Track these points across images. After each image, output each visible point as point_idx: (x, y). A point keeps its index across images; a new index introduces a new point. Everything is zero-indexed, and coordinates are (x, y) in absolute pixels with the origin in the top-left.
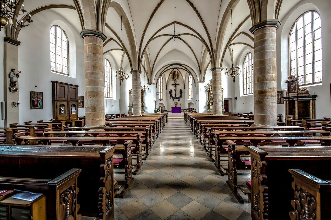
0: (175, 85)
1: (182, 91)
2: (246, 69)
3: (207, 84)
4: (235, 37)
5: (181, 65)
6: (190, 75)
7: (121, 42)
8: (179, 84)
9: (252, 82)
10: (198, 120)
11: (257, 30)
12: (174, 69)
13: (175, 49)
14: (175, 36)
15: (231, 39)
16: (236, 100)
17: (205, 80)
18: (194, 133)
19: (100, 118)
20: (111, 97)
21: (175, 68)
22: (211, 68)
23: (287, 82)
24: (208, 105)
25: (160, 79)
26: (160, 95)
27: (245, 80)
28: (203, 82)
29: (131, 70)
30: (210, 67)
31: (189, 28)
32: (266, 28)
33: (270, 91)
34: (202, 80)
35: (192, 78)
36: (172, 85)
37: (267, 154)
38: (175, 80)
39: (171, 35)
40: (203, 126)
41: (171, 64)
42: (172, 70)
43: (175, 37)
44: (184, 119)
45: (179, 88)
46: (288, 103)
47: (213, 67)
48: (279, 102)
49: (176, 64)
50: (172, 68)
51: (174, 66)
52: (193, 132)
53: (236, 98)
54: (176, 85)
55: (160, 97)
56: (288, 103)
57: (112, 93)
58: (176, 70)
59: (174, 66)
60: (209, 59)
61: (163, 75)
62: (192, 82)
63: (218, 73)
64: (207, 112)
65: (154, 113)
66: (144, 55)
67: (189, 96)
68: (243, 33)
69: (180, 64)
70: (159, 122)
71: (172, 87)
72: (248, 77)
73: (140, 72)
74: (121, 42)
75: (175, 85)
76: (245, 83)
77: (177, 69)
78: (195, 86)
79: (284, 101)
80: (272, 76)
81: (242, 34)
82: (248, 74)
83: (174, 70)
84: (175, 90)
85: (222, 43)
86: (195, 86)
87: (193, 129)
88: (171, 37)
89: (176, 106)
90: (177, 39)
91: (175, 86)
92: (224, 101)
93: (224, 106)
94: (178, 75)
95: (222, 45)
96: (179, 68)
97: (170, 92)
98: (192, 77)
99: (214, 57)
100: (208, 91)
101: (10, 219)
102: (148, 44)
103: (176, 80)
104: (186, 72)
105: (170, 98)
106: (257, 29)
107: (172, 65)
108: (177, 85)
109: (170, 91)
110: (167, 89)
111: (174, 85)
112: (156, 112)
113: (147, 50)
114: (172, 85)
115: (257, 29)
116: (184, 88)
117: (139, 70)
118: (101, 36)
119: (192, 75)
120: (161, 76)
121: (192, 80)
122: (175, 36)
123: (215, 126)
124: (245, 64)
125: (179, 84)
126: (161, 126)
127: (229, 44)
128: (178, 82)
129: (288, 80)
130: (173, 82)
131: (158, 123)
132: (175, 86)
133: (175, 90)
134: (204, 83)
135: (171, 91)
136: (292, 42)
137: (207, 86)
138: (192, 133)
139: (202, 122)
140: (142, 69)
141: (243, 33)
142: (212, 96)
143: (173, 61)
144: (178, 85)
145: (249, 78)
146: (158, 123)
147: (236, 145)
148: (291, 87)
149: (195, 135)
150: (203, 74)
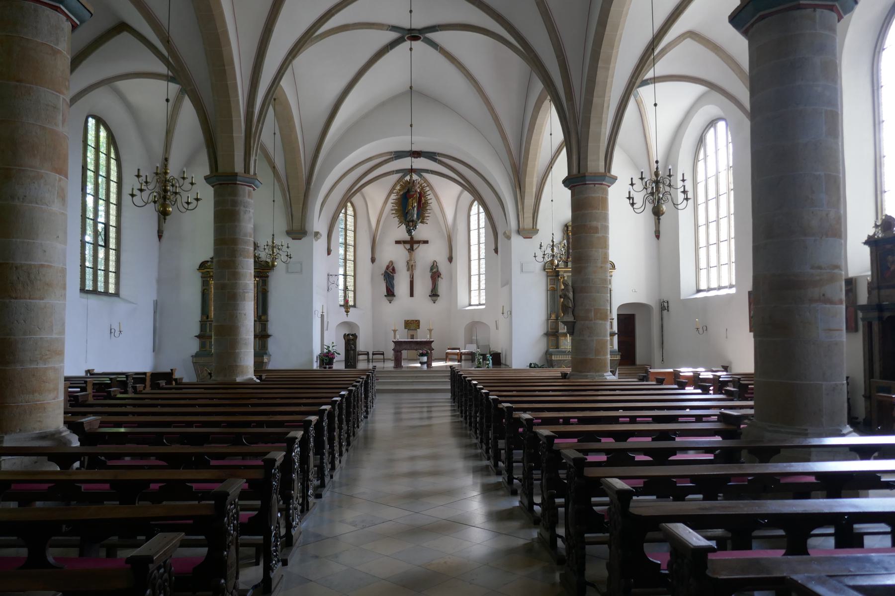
0: (411, 244)
1: (439, 270)
2: (704, 183)
3: (546, 242)
4: (664, 51)
5: (435, 160)
6: (476, 203)
7: (167, 41)
8: (426, 242)
9: (728, 240)
10: (500, 399)
11: (763, 18)
12: (404, 176)
13: (411, 88)
14: (414, 35)
15: (648, 56)
16: (665, 312)
17: (538, 227)
18: (496, 465)
19: (36, 394)
20: (112, 290)
21: (412, 171)
22: (565, 174)
23: (871, 242)
24: (552, 334)
25: (346, 213)
26: (341, 286)
27: (702, 231)
28: (528, 232)
29: (208, 172)
30: (561, 169)
31: (447, 167)
32: (797, 13)
33: (818, 278)
34: (527, 223)
35: (483, 216)
36: (397, 242)
37: (460, 372)
38: (409, 222)
39: (394, 28)
40: (484, 395)
41: (396, 152)
42: (397, 176)
43: (415, 38)
44: (449, 395)
45: (427, 255)
46: (876, 328)
47: (575, 171)
48: (852, 327)
49: (416, 154)
50: (398, 172)
51: (405, 163)
52: (466, 423)
53: (666, 304)
54: (415, 246)
55: (341, 293)
56: (876, 328)
57: (83, 267)
58: (415, 177)
59: (405, 163)
60: (559, 135)
61: (357, 199)
62: (483, 231)
63: (593, 195)
64: (529, 367)
65: (316, 366)
66: (271, 108)
67: (470, 291)
68: (692, 35)
69: (431, 156)
70: (337, 413)
71: (394, 253)
72: (712, 217)
73: (252, 182)
74: (167, 41)
75: (411, 244)
76: (702, 242)
77: (421, 176)
78: (496, 251)
79: (860, 324)
80: (827, 215)
81: (688, 41)
82: (712, 204)
83: (408, 178)
84: (411, 267)
85: (610, 72)
86: (496, 251)
87: (466, 413)
88: (393, 35)
89: (412, 337)
90: (418, 45)
91: (408, 246)
92: (618, 315)
93: (616, 336)
94: (423, 201)
95: (609, 80)
96: (427, 171)
97: (386, 272)
98: (481, 210)
99: (579, 128)
100: (552, 272)
101: (153, 523)
102: (291, 61)
103: (413, 221)
104: (459, 188)
105: (385, 298)
106: (762, 13)
107: (399, 155)
108: (419, 242)
109: (388, 267)
110: (373, 260)
111: (405, 242)
112: (176, 380)
113: (285, 83)
114: (397, 242)
115: (762, 13)
116: (450, 259)
117: (249, 172)
118: (253, 184)
119: (483, 203)
120: (349, 204)
121: (482, 224)
122: (414, 35)
123: (567, 421)
124: (701, 165)
125: (426, 242)
126: (348, 424)
127: (636, 80)
128: (422, 231)
129: (875, 234)
130: (401, 232)
131: (337, 408)
132: (411, 250)
133: (411, 267)
134: (537, 239)
135: (394, 269)
136: (714, 177)
137: (549, 251)
138: (458, 413)
139: (514, 406)
140: (258, 167)
141: (693, 38)
142: (571, 295)
143: (401, 142)
144: (422, 246)
145: (718, 221)
146: (337, 408)
147: (557, 438)
148: (889, 265)
149: (499, 473)
150: (529, 201)
